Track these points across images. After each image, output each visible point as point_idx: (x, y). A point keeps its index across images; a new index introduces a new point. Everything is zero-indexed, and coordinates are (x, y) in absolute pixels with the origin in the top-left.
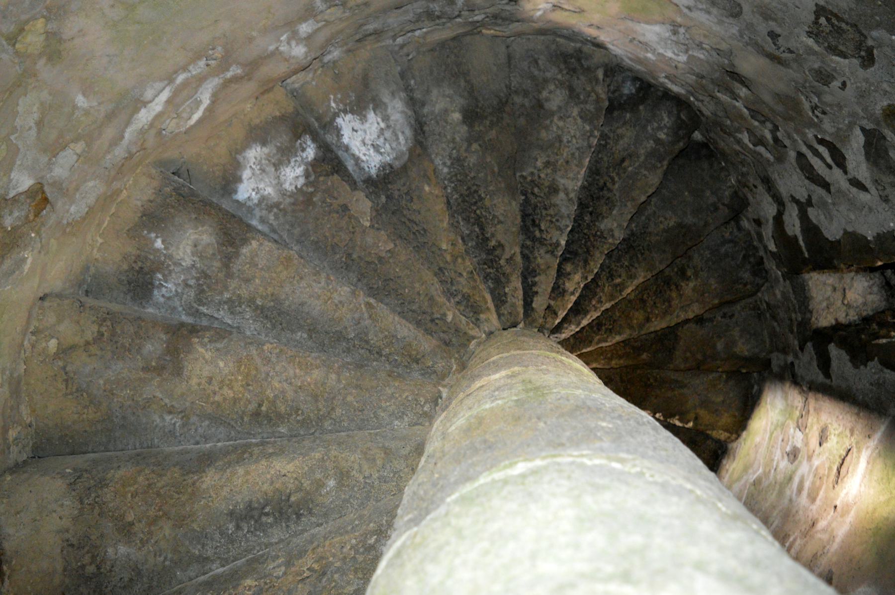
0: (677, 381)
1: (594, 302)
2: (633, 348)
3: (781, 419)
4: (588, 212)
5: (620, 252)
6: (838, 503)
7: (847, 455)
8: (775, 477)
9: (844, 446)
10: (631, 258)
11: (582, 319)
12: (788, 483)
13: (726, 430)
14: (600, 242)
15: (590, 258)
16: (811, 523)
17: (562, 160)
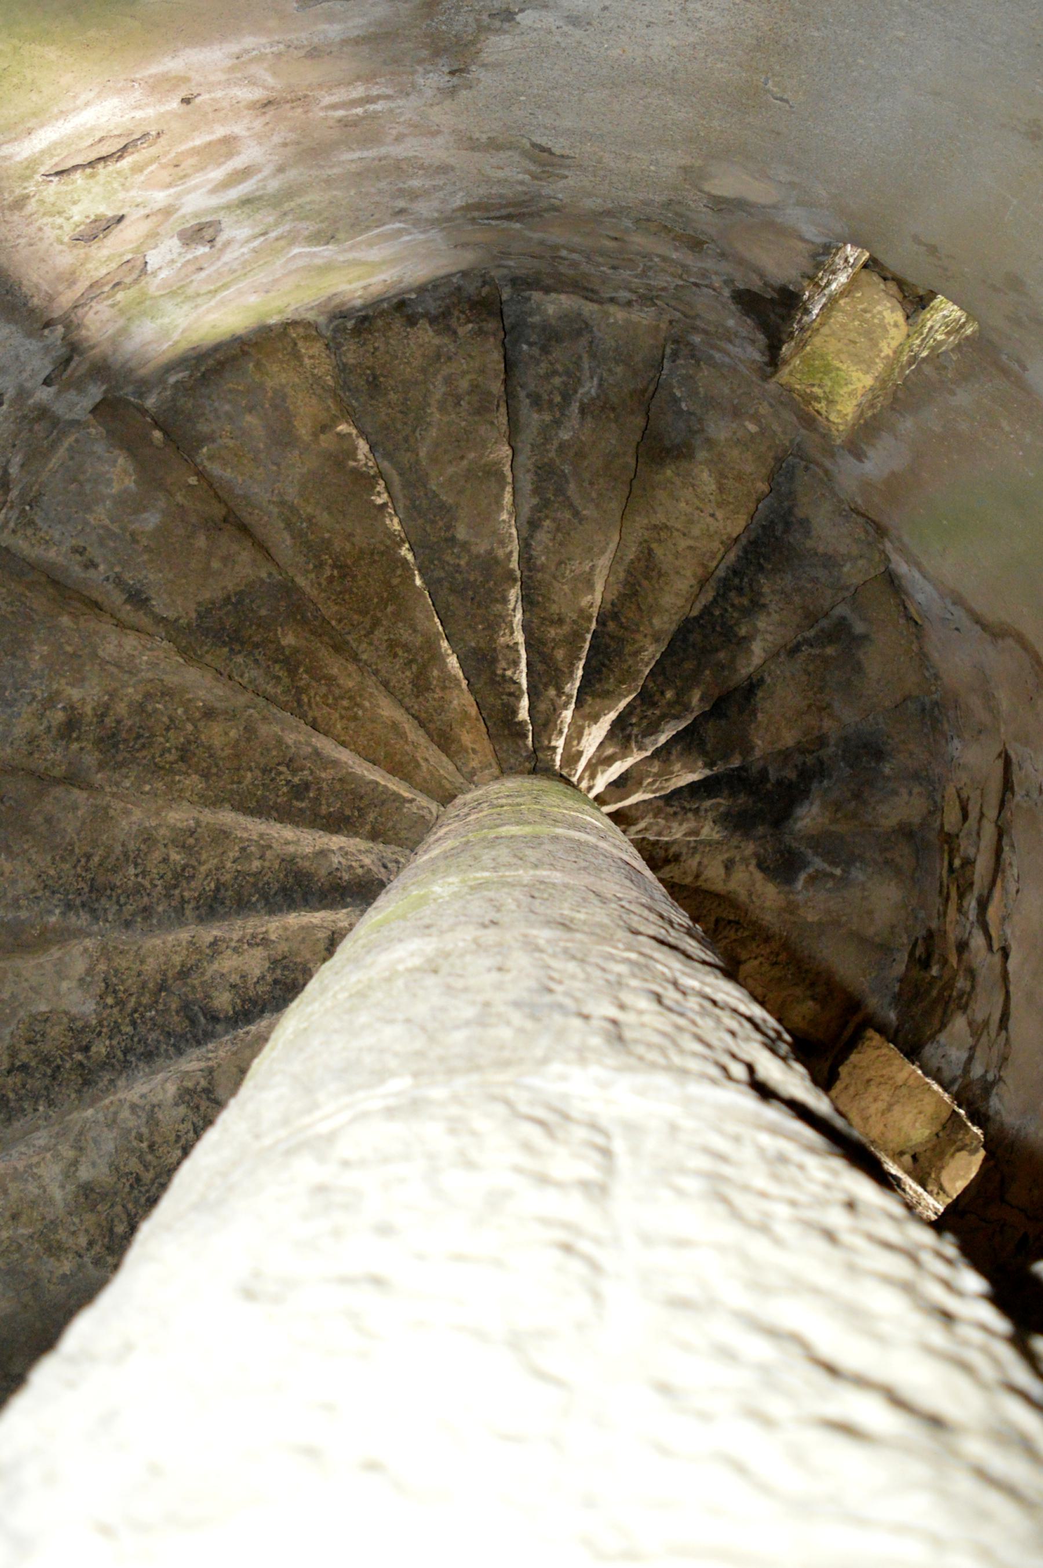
0: (289, 526)
1: (256, 865)
2: (292, 672)
3: (168, 305)
4: (88, 1058)
5: (122, 900)
6: (174, 104)
7: (75, 168)
8: (277, 224)
9: (64, 188)
10: (115, 870)
11: (305, 857)
12: (260, 198)
13: (297, 356)
14: (123, 982)
15: (170, 974)
16: (271, 112)
17: (22, 1231)
